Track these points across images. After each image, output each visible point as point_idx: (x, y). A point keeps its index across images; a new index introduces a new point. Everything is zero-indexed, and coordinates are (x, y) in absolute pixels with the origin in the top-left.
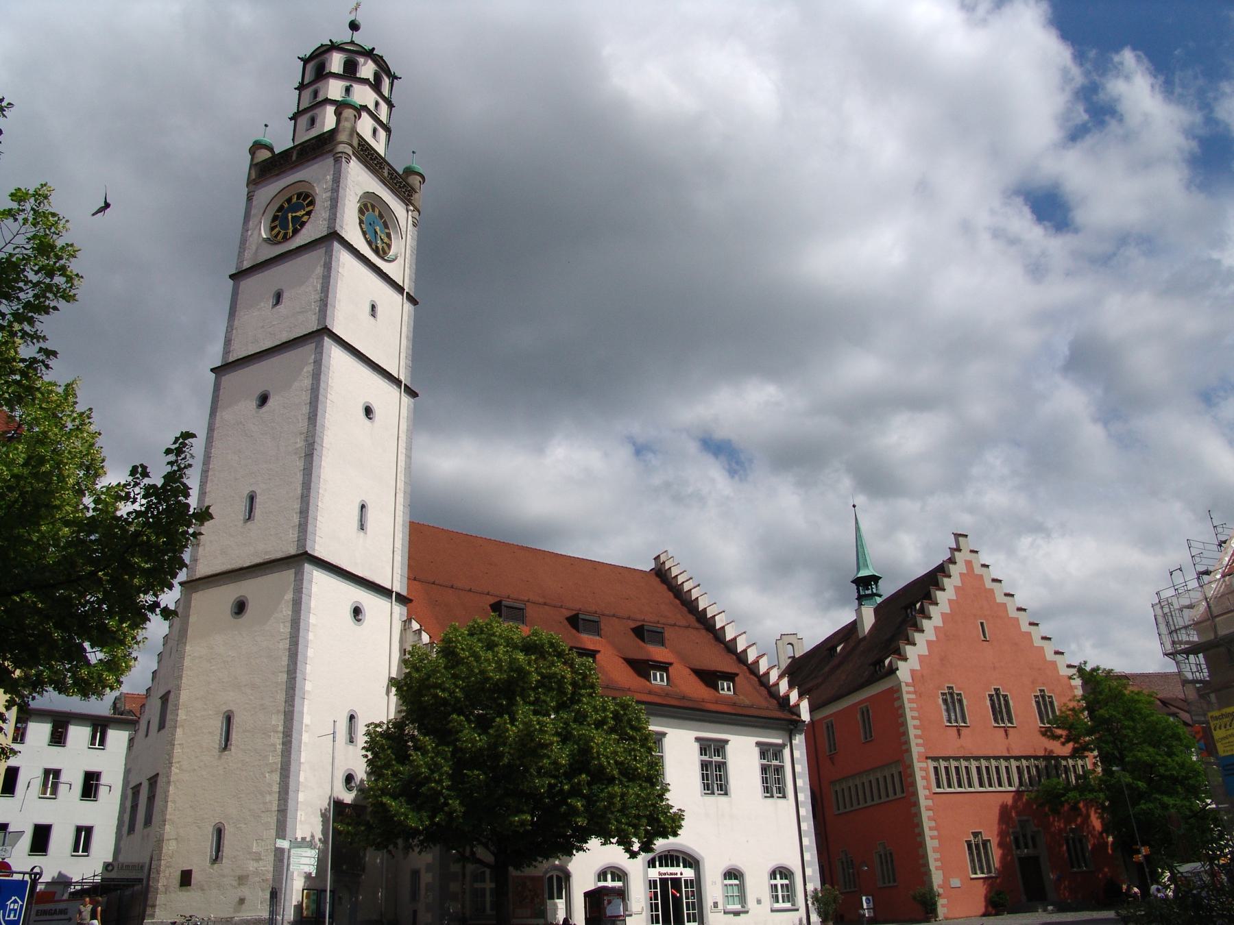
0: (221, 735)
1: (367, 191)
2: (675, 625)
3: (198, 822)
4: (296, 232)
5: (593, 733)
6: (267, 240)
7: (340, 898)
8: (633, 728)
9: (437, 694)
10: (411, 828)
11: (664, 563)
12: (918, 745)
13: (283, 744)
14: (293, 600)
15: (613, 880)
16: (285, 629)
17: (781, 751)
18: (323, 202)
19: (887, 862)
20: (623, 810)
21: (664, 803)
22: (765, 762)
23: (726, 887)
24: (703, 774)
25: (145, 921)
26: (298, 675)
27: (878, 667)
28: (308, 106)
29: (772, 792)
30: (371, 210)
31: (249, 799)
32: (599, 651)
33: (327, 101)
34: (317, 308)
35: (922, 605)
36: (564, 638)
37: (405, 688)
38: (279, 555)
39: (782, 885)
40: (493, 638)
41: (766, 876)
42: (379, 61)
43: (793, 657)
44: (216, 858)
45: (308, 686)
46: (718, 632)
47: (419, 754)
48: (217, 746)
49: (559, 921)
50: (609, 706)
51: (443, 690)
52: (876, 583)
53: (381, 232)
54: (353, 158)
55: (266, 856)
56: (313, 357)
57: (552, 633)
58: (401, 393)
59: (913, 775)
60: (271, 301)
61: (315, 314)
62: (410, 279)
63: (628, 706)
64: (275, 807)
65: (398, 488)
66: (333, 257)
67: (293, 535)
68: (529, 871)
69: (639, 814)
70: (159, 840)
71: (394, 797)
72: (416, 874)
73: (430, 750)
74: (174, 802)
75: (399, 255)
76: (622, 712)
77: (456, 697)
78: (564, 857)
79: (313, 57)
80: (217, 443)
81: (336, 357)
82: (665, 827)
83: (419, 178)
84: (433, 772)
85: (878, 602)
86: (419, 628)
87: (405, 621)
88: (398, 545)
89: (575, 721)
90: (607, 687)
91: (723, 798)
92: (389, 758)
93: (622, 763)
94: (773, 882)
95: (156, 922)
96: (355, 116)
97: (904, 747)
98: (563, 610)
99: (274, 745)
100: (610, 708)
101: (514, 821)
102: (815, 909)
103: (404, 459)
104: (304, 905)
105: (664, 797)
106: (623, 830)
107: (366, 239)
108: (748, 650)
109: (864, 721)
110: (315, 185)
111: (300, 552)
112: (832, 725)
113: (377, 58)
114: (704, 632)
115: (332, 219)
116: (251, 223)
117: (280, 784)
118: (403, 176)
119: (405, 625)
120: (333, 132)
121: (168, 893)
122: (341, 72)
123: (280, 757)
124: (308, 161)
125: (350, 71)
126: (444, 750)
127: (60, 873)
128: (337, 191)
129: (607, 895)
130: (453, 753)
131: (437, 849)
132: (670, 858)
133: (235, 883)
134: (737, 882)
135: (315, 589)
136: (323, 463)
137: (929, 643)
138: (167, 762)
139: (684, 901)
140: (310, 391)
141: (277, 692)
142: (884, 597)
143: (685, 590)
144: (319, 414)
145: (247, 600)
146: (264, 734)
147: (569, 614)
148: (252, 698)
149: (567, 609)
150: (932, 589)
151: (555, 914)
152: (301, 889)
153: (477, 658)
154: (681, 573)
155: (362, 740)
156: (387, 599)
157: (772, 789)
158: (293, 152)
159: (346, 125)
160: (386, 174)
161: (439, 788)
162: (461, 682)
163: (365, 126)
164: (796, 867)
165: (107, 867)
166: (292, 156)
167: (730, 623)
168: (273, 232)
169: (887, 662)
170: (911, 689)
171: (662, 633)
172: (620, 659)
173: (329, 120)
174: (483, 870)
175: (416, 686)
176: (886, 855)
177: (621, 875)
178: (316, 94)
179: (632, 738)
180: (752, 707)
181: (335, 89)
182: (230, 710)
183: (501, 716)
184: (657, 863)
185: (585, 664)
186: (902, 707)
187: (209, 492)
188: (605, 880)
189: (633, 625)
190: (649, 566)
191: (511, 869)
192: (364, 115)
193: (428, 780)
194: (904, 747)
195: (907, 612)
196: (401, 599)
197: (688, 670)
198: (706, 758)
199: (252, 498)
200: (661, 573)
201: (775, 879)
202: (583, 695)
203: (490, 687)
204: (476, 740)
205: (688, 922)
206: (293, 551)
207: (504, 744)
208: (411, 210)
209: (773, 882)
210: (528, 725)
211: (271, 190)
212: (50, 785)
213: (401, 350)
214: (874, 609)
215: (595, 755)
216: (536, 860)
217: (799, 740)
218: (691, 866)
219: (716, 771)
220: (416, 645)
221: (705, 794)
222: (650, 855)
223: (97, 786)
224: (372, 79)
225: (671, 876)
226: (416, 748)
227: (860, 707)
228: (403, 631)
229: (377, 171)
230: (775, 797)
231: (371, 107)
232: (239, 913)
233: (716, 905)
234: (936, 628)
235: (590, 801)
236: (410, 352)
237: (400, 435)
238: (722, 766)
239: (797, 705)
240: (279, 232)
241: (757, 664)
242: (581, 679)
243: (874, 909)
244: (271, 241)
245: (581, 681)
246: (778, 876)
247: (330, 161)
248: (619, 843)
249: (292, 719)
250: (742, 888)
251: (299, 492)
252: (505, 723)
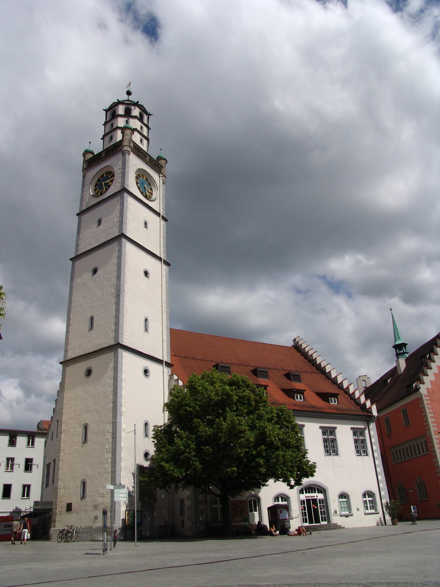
0: (83, 435)
1: (139, 168)
2: (306, 372)
3: (74, 479)
4: (107, 190)
5: (266, 424)
6: (93, 196)
7: (145, 515)
8: (287, 421)
9: (187, 409)
10: (176, 477)
11: (298, 342)
12: (433, 426)
13: (112, 438)
14: (114, 367)
15: (282, 501)
16: (110, 381)
17: (364, 432)
18: (118, 175)
19: (422, 487)
20: (284, 463)
21: (305, 460)
22: (356, 437)
23: (341, 508)
24: (325, 445)
25: (51, 529)
26: (118, 404)
27: (409, 388)
28: (109, 131)
29: (361, 453)
30: (141, 177)
31: (98, 467)
32: (268, 386)
33: (118, 128)
34: (118, 225)
35: (430, 356)
36: (251, 380)
37: (171, 407)
38: (106, 345)
39: (369, 501)
40: (214, 380)
41: (361, 496)
42: (141, 107)
43: (366, 387)
44: (83, 497)
45: (123, 409)
46: (328, 374)
47: (179, 439)
48: (81, 441)
49: (256, 523)
50: (274, 410)
51: (190, 407)
52: (405, 347)
53: (147, 187)
54: (131, 153)
55: (106, 495)
56: (118, 248)
57: (243, 375)
58: (162, 264)
59: (432, 442)
60: (96, 225)
61: (117, 228)
62: (163, 209)
63: (284, 410)
64: (110, 470)
65: (163, 310)
66: (124, 200)
67: (112, 335)
68: (238, 498)
69: (292, 465)
70: (56, 489)
71: (167, 462)
72: (182, 501)
73: (185, 437)
74: (62, 470)
75: (157, 198)
76: (280, 413)
77: (196, 410)
78: (257, 489)
79: (110, 108)
80: (74, 294)
81: (129, 247)
82: (307, 472)
83: (164, 161)
84: (186, 448)
85: (407, 357)
86: (177, 378)
87: (170, 376)
88: (165, 338)
89: (257, 419)
90: (273, 403)
91: (336, 457)
92: (165, 443)
93: (282, 439)
94: (365, 499)
95: (56, 529)
96: (131, 133)
97: (426, 428)
98: (249, 367)
99: (108, 439)
100: (274, 412)
101: (228, 471)
102: (388, 513)
103: (165, 296)
104: (127, 520)
105: (305, 456)
106: (285, 474)
107: (140, 191)
108: (343, 382)
109: (404, 416)
110: (114, 167)
111: (116, 343)
112: (388, 419)
113: (140, 106)
114: (320, 375)
115: (123, 182)
116: (85, 189)
117: (112, 458)
118: (156, 160)
119: (170, 377)
120: (121, 141)
121: (61, 514)
122: (124, 114)
123: (111, 445)
124: (110, 156)
125: (128, 114)
126: (191, 437)
127: (16, 507)
128: (125, 169)
129: (279, 508)
130: (196, 438)
131: (192, 487)
132: (310, 489)
133: (92, 509)
134: (346, 500)
135: (124, 361)
136: (125, 299)
137: (435, 374)
138: (58, 450)
139: (319, 510)
140: (117, 265)
141: (108, 413)
142: (410, 354)
143: (309, 355)
144: (121, 275)
145: (89, 369)
146: (103, 434)
147: (252, 369)
148: (97, 416)
149: (251, 366)
150: (421, 375)
151: (254, 519)
152: (125, 511)
153: (206, 390)
154: (307, 346)
155: (151, 433)
156: (161, 365)
157: (360, 451)
158: (103, 153)
159: (127, 137)
160: (148, 160)
161: (189, 456)
162: (199, 403)
163: (136, 137)
164: (375, 490)
165: (36, 503)
166: (102, 155)
167: (333, 369)
168: (96, 192)
169: (414, 385)
170: (428, 398)
171: (299, 376)
172: (279, 389)
173: (119, 136)
174: (216, 498)
175: (177, 405)
176: (421, 484)
177: (286, 498)
178: (112, 125)
179: (287, 427)
180: (347, 410)
181: (121, 122)
182: (86, 423)
183: (219, 418)
184: (304, 492)
185: (261, 391)
186: (424, 407)
187: (72, 318)
188: (278, 501)
189: (285, 373)
190: (290, 344)
191: (229, 497)
192: (136, 133)
193: (184, 452)
194: (426, 428)
195: (422, 360)
196: (168, 365)
197: (314, 393)
198: (326, 437)
199: (92, 319)
200: (297, 347)
201: (365, 497)
202: (261, 407)
203: (213, 403)
204: (207, 431)
205: (322, 521)
206: (112, 343)
207: (221, 432)
208: (161, 176)
209: (365, 499)
210: (232, 421)
211: (93, 172)
212: (10, 466)
213: (161, 244)
214: (405, 360)
215: (268, 436)
216: (242, 492)
217: (373, 426)
218: (321, 493)
219: (331, 443)
220: (176, 385)
221: (326, 455)
222: (300, 487)
223: (31, 465)
224: (138, 116)
225: (312, 498)
226: (178, 437)
227: (401, 409)
228: (170, 380)
229: (144, 158)
230: (362, 455)
231: (139, 129)
232: (95, 523)
233: (336, 512)
234: (431, 382)
235: (267, 459)
236: (165, 244)
237: (163, 284)
238: (334, 441)
239: (370, 408)
240: (99, 191)
241: (348, 389)
242: (259, 398)
243: (417, 512)
244: (95, 196)
245: (259, 400)
246: (367, 496)
247: (120, 155)
248: (284, 481)
249: (116, 426)
250: (348, 503)
251: (114, 314)
252: (221, 421)
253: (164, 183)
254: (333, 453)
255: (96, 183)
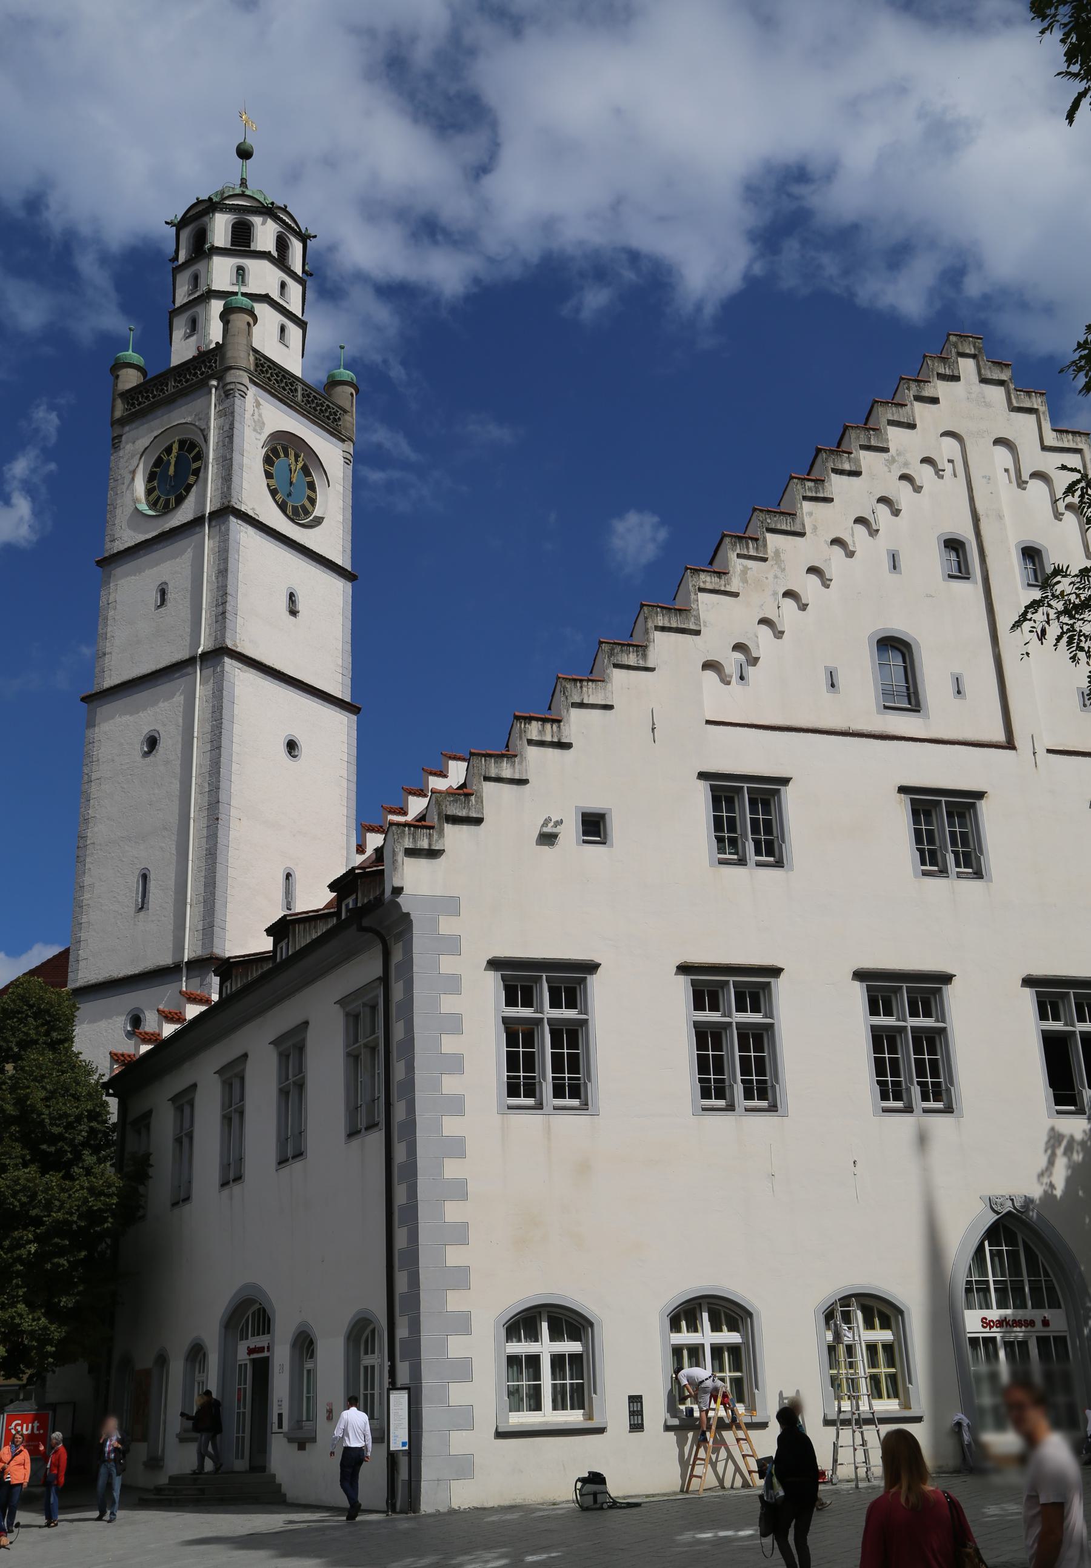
41: (656, 1321)
125: (242, 235)
168: (151, 498)
178: (196, 278)
224: (275, 254)
231: (275, 295)
240: (159, 498)
253: (347, 461)
254: (958, 865)
255: (151, 471)
